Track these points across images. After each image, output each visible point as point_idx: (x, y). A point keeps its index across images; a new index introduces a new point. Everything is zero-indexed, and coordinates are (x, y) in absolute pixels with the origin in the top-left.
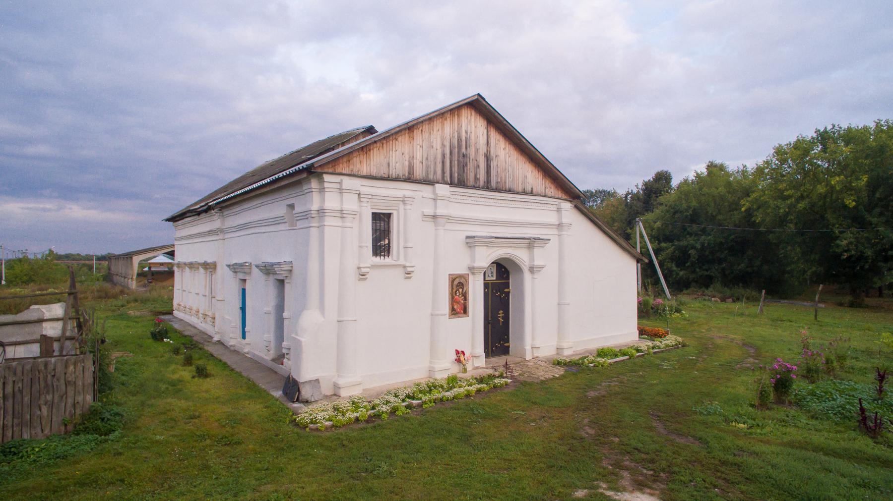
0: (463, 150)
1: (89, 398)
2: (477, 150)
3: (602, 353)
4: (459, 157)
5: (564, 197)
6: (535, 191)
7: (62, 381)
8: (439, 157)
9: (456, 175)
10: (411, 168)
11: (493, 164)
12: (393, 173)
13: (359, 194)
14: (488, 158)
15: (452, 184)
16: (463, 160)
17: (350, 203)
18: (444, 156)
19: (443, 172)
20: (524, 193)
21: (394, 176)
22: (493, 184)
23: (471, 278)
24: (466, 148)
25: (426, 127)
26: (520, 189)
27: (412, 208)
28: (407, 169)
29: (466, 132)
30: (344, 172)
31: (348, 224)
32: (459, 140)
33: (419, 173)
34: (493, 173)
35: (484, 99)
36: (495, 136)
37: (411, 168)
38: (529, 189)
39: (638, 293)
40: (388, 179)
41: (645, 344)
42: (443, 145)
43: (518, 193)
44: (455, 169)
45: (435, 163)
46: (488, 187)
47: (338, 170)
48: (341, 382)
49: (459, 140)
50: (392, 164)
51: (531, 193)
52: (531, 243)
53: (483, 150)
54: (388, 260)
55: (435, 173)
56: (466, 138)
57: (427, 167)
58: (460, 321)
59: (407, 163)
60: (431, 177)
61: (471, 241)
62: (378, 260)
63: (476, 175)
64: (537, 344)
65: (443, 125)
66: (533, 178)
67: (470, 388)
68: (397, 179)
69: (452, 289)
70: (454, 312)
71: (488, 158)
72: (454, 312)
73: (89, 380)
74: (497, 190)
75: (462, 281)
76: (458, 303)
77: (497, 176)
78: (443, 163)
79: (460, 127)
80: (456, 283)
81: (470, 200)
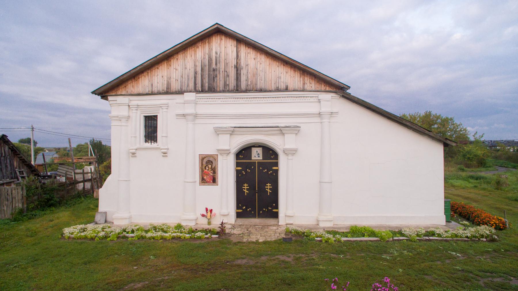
0: (214, 66)
1: (20, 205)
2: (226, 64)
3: (355, 231)
4: (209, 71)
5: (328, 89)
6: (290, 87)
7: (11, 197)
8: (192, 75)
9: (207, 85)
10: (169, 85)
11: (243, 72)
12: (155, 90)
13: (129, 106)
14: (238, 68)
15: (196, 91)
16: (213, 73)
17: (123, 112)
18: (196, 73)
19: (195, 84)
20: (278, 90)
21: (156, 92)
22: (243, 86)
23: (220, 158)
24: (216, 64)
25: (180, 56)
26: (273, 87)
27: (170, 112)
28: (165, 86)
29: (216, 53)
30: (123, 93)
31: (123, 124)
32: (210, 60)
33: (175, 86)
34: (243, 78)
35: (223, 26)
36: (243, 50)
37: (169, 85)
38: (283, 86)
39: (105, 180)
40: (152, 94)
41: (463, 230)
42: (195, 66)
43: (270, 91)
44: (206, 80)
45: (188, 79)
46: (237, 89)
47: (119, 93)
48: (321, 218)
49: (210, 60)
50: (155, 84)
51: (287, 89)
52: (281, 130)
53: (234, 62)
54: (154, 145)
55: (188, 86)
56: (216, 58)
57: (181, 82)
58: (209, 188)
59: (166, 82)
60: (184, 89)
61: (218, 131)
62: (148, 145)
63: (225, 83)
64: (289, 213)
65: (195, 52)
66: (291, 78)
67: (181, 235)
68: (159, 93)
69: (202, 164)
70: (203, 181)
71: (238, 68)
72: (203, 181)
73: (20, 198)
74: (246, 91)
75: (211, 159)
76: (208, 174)
77: (247, 80)
78: (195, 78)
79: (210, 50)
80: (205, 160)
81: (219, 101)
